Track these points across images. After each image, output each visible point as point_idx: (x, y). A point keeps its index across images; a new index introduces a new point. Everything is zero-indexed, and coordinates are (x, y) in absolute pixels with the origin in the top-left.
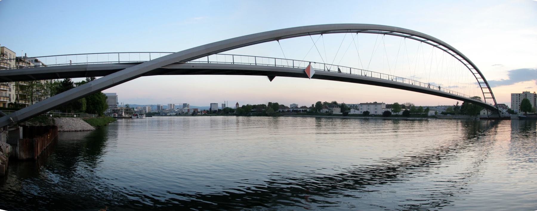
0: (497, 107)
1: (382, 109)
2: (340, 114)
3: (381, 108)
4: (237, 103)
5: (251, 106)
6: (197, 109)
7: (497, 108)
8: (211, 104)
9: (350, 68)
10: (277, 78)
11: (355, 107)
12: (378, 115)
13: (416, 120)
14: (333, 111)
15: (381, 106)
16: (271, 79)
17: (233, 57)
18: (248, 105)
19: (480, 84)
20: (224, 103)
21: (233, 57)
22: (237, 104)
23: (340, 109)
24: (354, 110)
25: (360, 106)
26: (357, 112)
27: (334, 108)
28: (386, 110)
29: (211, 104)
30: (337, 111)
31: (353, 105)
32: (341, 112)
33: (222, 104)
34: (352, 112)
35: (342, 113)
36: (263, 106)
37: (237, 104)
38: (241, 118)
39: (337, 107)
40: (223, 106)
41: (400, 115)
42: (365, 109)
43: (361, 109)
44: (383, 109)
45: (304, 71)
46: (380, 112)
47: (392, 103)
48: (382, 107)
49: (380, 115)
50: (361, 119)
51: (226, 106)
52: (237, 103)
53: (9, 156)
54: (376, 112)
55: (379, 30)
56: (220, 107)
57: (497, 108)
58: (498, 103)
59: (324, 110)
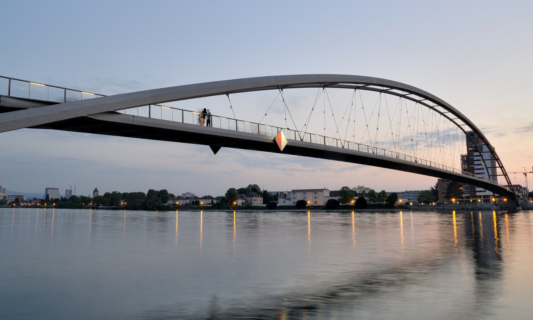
0: (513, 190)
1: (324, 197)
2: (262, 207)
3: (323, 197)
4: (96, 188)
5: (119, 193)
6: (23, 196)
7: (512, 191)
8: (47, 189)
9: (324, 137)
10: (223, 151)
11: (284, 195)
12: (320, 206)
13: (388, 211)
14: (252, 203)
15: (323, 193)
16: (215, 150)
17: (295, 133)
18: (114, 192)
19: (485, 161)
20: (69, 189)
21: (295, 133)
22: (96, 191)
23: (262, 199)
24: (283, 200)
25: (292, 194)
26: (288, 203)
27: (253, 198)
28: (331, 198)
29: (47, 189)
30: (258, 201)
31: (281, 193)
32: (264, 203)
33: (67, 190)
34: (281, 202)
35: (265, 205)
36: (141, 194)
37: (96, 191)
38: (101, 213)
39: (258, 196)
40: (68, 194)
41: (351, 206)
42: (299, 197)
43: (294, 198)
44: (326, 198)
45: (274, 140)
46: (322, 202)
47: (338, 188)
48: (325, 195)
49: (323, 206)
50: (294, 212)
51: (73, 194)
52: (96, 188)
53: (246, 204)
54: (316, 202)
55: (356, 83)
56: (62, 194)
57: (512, 191)
58: (513, 183)
59: (239, 202)
